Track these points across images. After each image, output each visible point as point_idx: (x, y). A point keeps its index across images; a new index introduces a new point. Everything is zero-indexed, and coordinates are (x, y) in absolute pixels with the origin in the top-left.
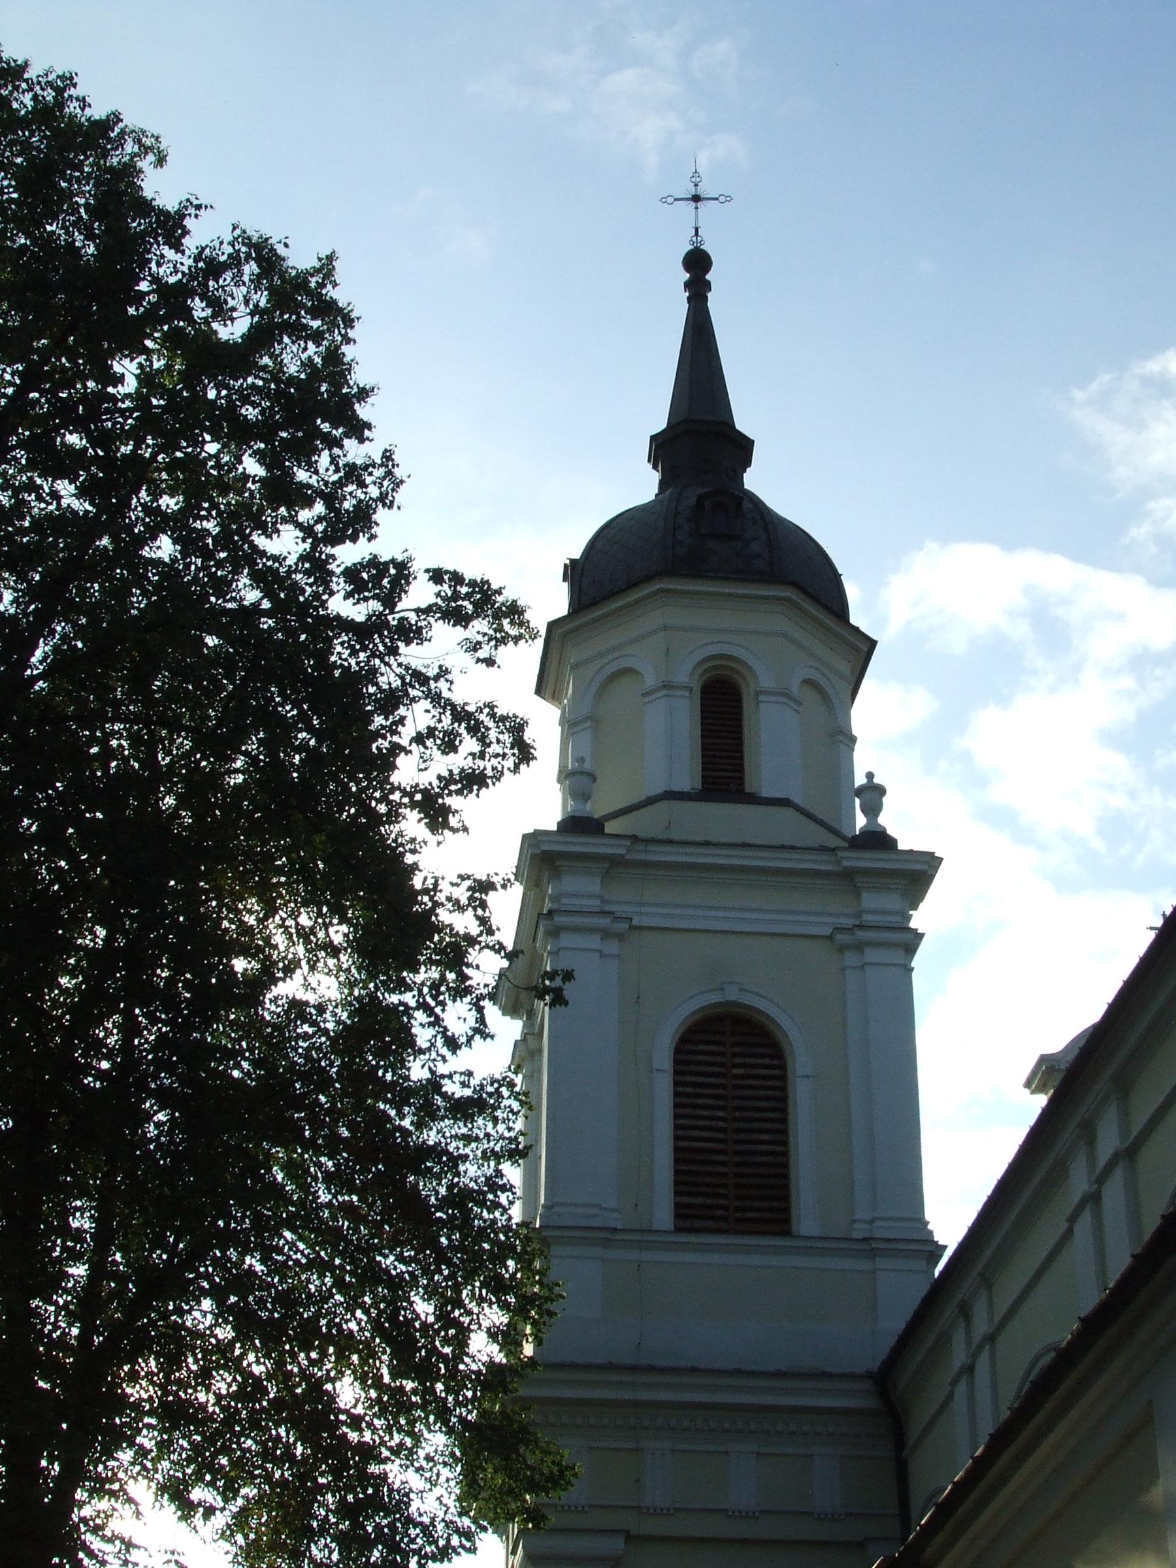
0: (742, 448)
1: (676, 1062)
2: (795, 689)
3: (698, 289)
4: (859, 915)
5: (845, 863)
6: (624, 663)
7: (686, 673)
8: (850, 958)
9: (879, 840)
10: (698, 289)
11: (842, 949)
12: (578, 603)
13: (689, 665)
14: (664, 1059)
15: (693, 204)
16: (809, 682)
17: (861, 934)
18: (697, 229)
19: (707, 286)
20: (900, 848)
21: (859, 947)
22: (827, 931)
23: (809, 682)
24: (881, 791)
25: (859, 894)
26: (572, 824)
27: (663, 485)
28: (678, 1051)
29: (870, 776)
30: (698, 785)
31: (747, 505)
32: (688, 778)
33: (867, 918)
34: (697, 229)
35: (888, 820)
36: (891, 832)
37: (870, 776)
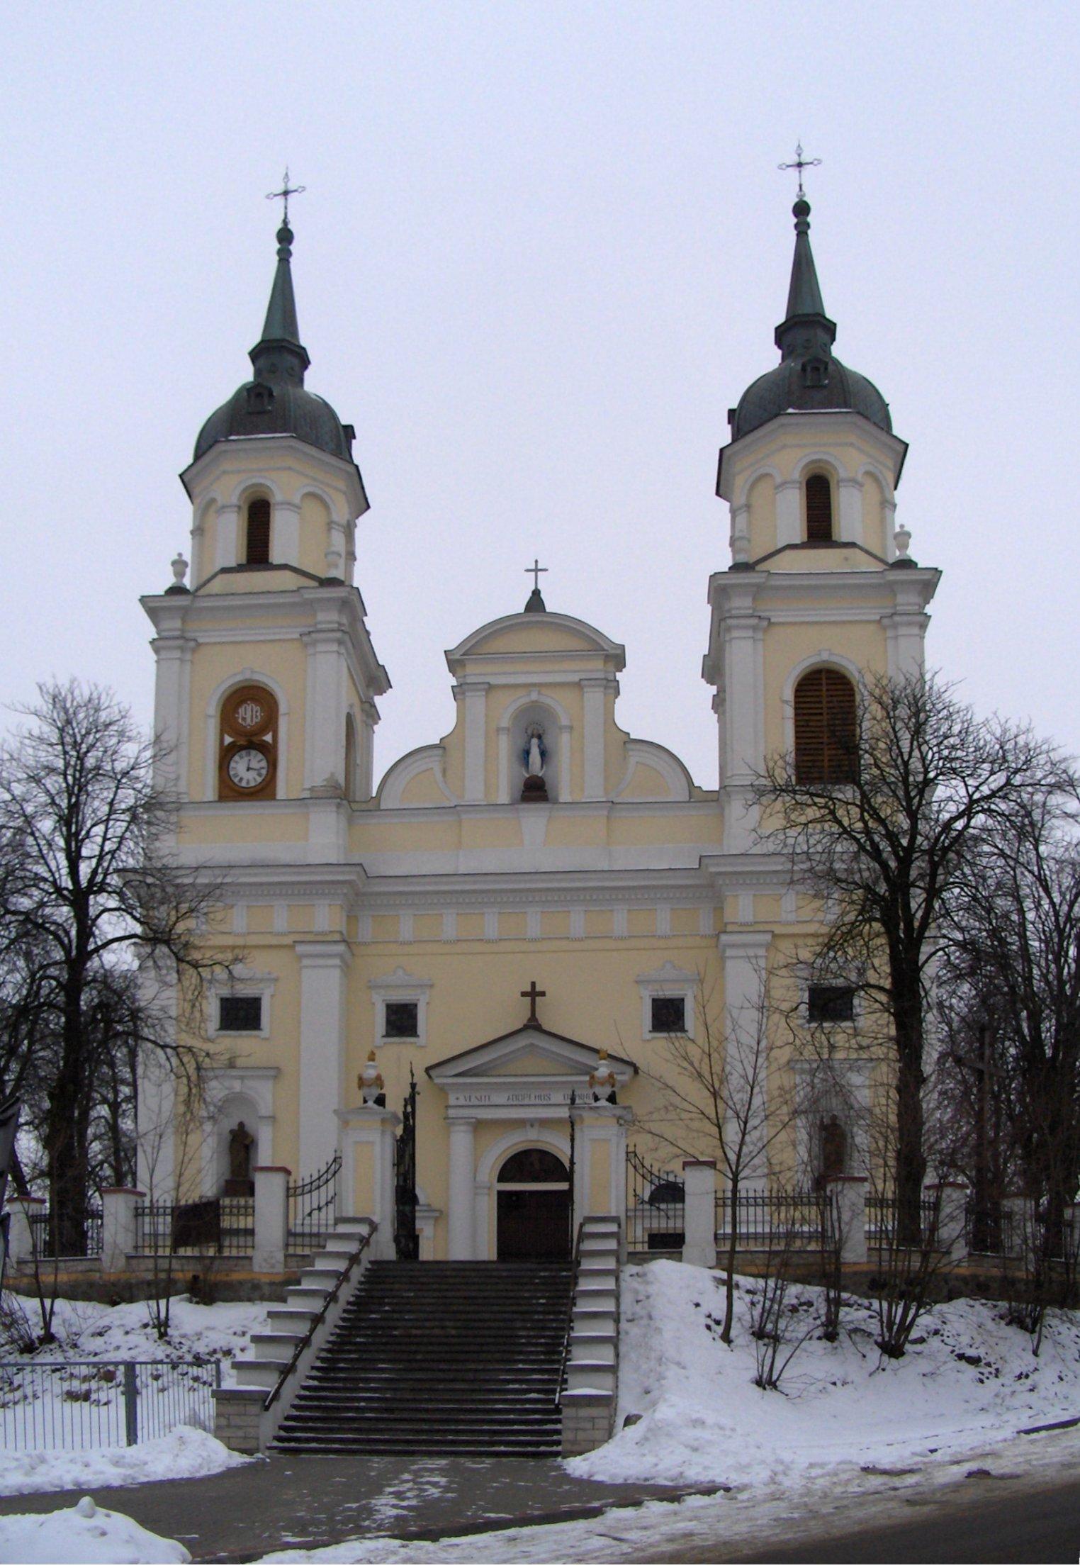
0: (830, 329)
1: (796, 697)
2: (860, 478)
3: (802, 229)
4: (895, 606)
5: (306, 596)
6: (762, 471)
7: (797, 474)
8: (890, 633)
9: (907, 564)
10: (802, 229)
11: (884, 628)
12: (737, 436)
13: (238, 492)
14: (789, 694)
15: (797, 169)
16: (868, 473)
17: (897, 618)
18: (801, 186)
19: (289, 253)
20: (919, 566)
21: (314, 643)
22: (297, 636)
23: (868, 473)
24: (908, 535)
25: (895, 595)
26: (736, 568)
27: (783, 358)
28: (797, 691)
29: (902, 526)
30: (805, 539)
31: (831, 367)
32: (799, 535)
33: (319, 626)
34: (801, 186)
35: (913, 553)
36: (914, 559)
37: (902, 526)
